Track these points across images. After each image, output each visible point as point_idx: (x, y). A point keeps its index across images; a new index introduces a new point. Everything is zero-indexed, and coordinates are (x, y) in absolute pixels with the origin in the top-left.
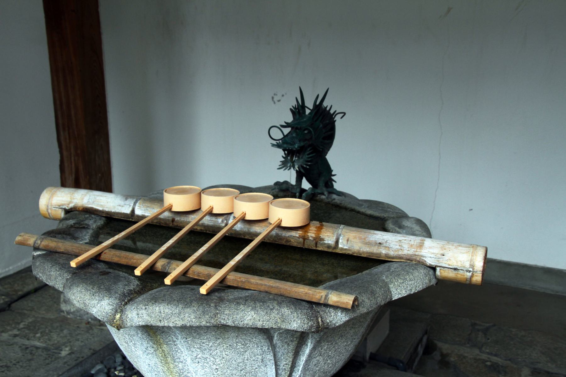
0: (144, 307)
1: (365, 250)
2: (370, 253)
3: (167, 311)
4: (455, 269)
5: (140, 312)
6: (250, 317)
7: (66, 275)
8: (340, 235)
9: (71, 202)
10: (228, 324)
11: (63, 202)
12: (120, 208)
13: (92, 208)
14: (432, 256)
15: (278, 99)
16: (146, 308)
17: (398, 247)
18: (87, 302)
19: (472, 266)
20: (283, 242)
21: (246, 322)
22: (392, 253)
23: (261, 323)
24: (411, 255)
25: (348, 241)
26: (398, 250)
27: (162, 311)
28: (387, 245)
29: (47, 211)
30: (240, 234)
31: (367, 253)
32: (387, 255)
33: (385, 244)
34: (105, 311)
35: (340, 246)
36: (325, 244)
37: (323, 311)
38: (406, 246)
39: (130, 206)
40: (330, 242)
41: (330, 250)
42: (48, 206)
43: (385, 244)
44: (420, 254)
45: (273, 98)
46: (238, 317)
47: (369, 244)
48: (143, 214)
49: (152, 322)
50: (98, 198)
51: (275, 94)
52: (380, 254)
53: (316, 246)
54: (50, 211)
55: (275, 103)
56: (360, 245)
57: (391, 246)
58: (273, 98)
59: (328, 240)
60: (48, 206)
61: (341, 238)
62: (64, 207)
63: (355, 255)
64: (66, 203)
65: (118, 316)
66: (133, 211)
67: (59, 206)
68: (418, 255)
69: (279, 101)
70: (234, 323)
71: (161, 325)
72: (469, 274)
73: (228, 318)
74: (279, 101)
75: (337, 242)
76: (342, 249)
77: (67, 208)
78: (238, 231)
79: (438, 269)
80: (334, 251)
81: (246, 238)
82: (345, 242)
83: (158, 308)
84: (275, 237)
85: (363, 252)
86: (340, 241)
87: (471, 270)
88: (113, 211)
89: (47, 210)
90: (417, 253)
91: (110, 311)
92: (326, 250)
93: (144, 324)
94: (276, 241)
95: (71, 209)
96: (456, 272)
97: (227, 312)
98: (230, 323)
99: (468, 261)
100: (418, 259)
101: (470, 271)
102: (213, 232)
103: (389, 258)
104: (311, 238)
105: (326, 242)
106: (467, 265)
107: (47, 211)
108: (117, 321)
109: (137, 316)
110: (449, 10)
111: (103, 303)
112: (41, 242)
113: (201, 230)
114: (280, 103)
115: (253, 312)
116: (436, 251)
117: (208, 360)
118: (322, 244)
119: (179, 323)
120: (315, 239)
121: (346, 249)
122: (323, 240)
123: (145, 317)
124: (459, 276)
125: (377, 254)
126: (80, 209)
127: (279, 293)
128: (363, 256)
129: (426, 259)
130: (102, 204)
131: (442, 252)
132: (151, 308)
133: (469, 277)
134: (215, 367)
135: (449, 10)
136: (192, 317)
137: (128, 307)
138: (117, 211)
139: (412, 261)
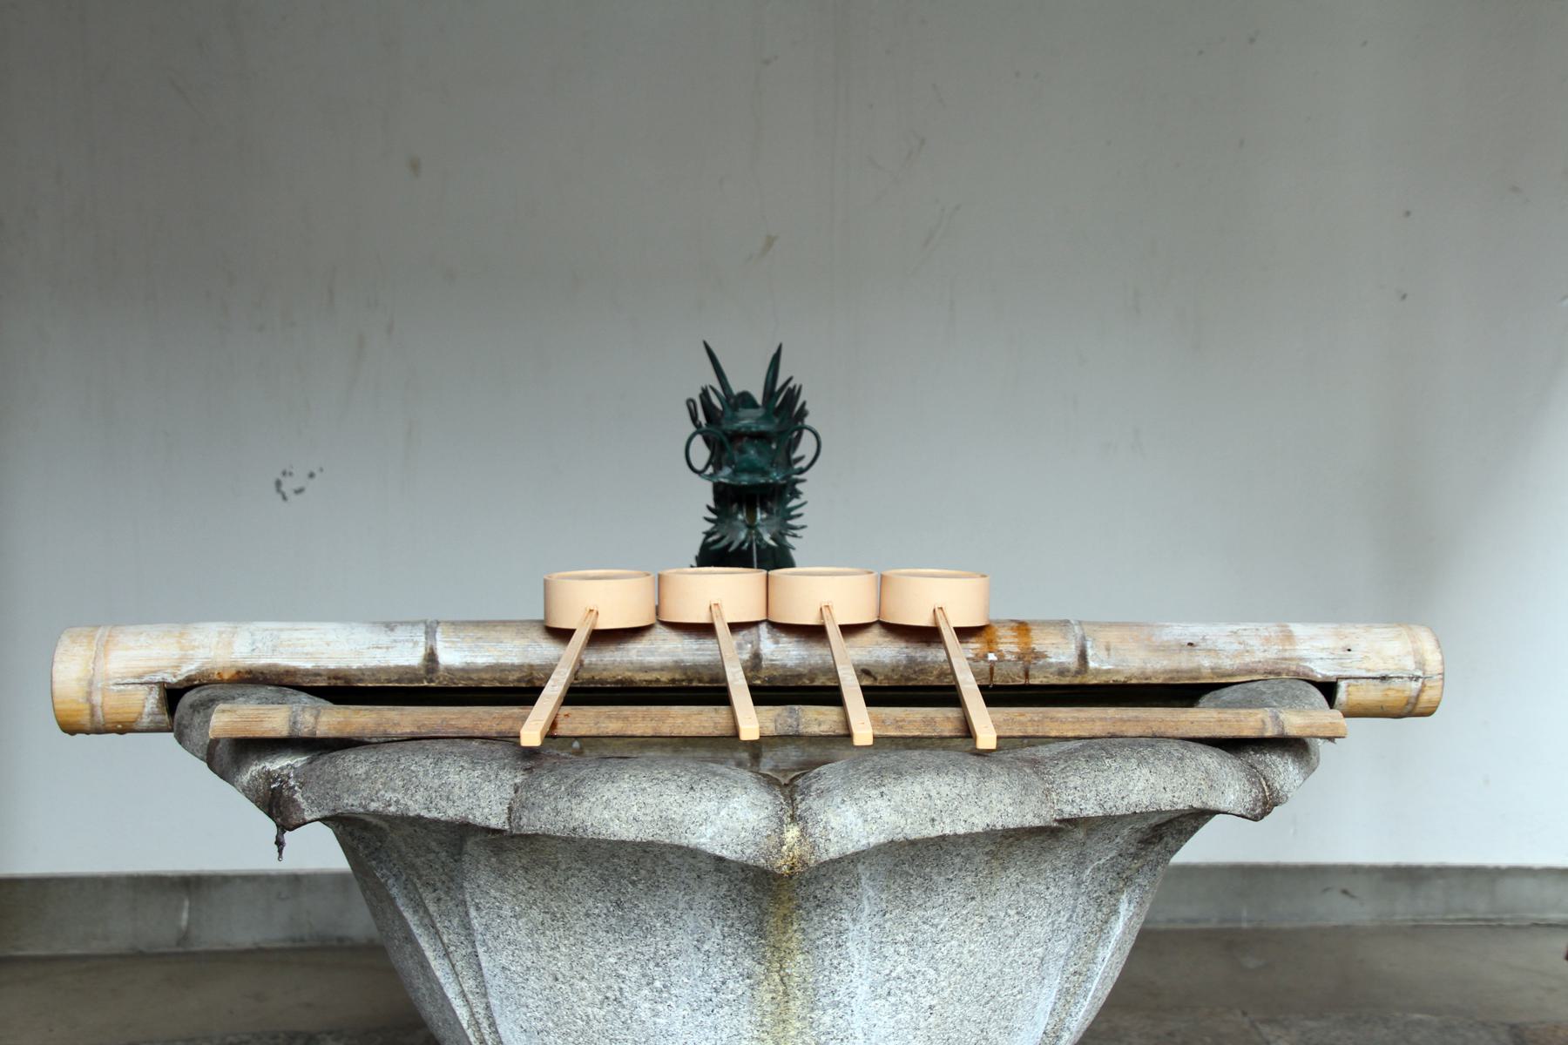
0: (874, 793)
1: (1158, 666)
2: (1171, 671)
3: (945, 790)
4: (1384, 678)
5: (869, 807)
6: (1141, 785)
7: (505, 775)
8: (1084, 638)
9: (184, 659)
10: (1084, 814)
11: (153, 664)
12: (379, 653)
13: (275, 665)
14: (1323, 655)
15: (297, 486)
16: (882, 794)
17: (1236, 646)
18: (676, 813)
19: (1421, 664)
20: (932, 680)
21: (1134, 798)
22: (1227, 664)
23: (1169, 795)
24: (1276, 661)
25: (1108, 649)
26: (1239, 654)
27: (933, 793)
28: (1210, 645)
29: (89, 700)
30: (800, 676)
31: (1165, 672)
32: (1215, 671)
33: (1203, 645)
34: (748, 826)
35: (1092, 664)
36: (1051, 665)
37: (1260, 763)
38: (1255, 643)
39: (416, 643)
40: (1063, 659)
41: (1066, 681)
42: (91, 683)
43: (1203, 645)
44: (1295, 654)
45: (278, 484)
46: (1112, 788)
47: (1164, 649)
48: (469, 660)
49: (908, 831)
50: (284, 636)
51: (284, 473)
52: (1198, 670)
53: (1027, 675)
54: (97, 699)
55: (285, 498)
56: (1143, 654)
57: (1220, 645)
58: (278, 484)
59: (1057, 655)
60: (91, 683)
61: (1089, 644)
62: (158, 678)
63: (1134, 681)
64: (164, 663)
65: (792, 834)
66: (431, 657)
67: (140, 677)
68: (1291, 659)
69: (299, 491)
70: (1101, 806)
71: (934, 834)
72: (1416, 686)
73: (1082, 798)
74: (299, 491)
75: (1083, 656)
76: (1098, 672)
77: (171, 679)
78: (790, 669)
79: (1343, 684)
80: (1077, 681)
81: (817, 683)
82: (1103, 654)
83: (917, 788)
84: (906, 667)
85: (1155, 672)
86: (1090, 652)
87: (1419, 673)
88: (355, 665)
89: (89, 699)
90: (1287, 655)
91: (764, 823)
92: (1054, 680)
93: (882, 839)
94: (908, 679)
95: (189, 679)
96: (1385, 685)
97: (1075, 781)
98: (1091, 810)
99: (1409, 653)
100: (1294, 668)
101: (1418, 678)
102: (712, 681)
103: (1223, 676)
104: (1008, 657)
105: (1053, 660)
106: (1410, 665)
107: (89, 700)
108: (790, 850)
109: (860, 821)
110: (770, 242)
111: (734, 803)
112: (316, 718)
113: (673, 681)
114: (300, 496)
115: (1145, 771)
116: (1329, 643)
117: (919, 979)
118: (1042, 667)
119: (980, 823)
120: (1020, 657)
121: (1108, 672)
122: (1040, 656)
123: (885, 819)
124: (1392, 694)
125: (1191, 671)
126: (226, 676)
127: (1149, 732)
128: (1154, 681)
129: (1311, 666)
130: (306, 649)
131: (1342, 644)
132: (898, 789)
133: (1414, 694)
134: (929, 1000)
135: (770, 242)
136: (1008, 801)
137: (809, 803)
138: (372, 663)
139: (1279, 674)
